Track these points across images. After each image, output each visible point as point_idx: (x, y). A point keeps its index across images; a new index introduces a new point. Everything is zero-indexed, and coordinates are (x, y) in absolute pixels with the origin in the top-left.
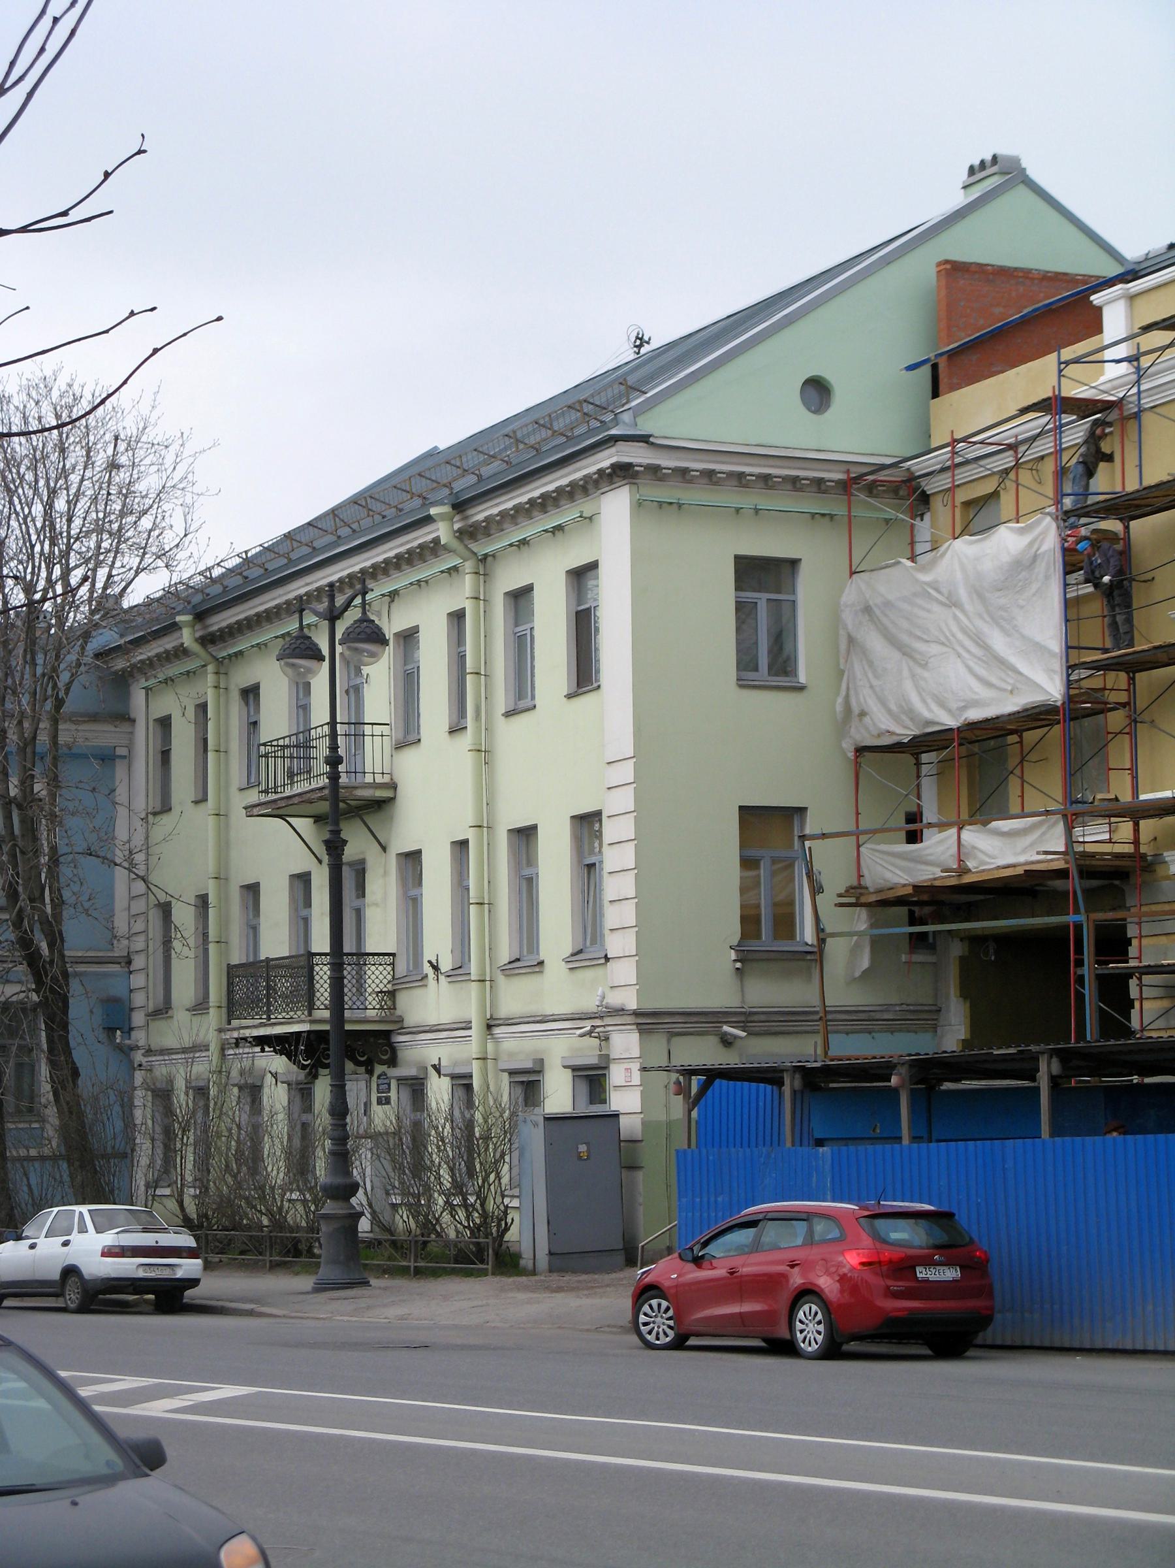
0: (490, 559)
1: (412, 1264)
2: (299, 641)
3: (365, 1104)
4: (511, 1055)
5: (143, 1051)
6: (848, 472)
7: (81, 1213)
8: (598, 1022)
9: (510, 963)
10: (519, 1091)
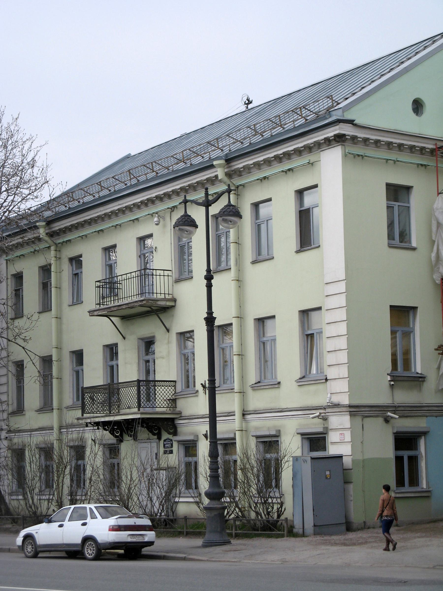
0: (240, 187)
1: (234, 532)
2: (227, 208)
3: (156, 454)
4: (257, 428)
5: (6, 431)
6: (436, 144)
7: (90, 508)
8: (322, 411)
9: (256, 383)
10: (261, 447)
